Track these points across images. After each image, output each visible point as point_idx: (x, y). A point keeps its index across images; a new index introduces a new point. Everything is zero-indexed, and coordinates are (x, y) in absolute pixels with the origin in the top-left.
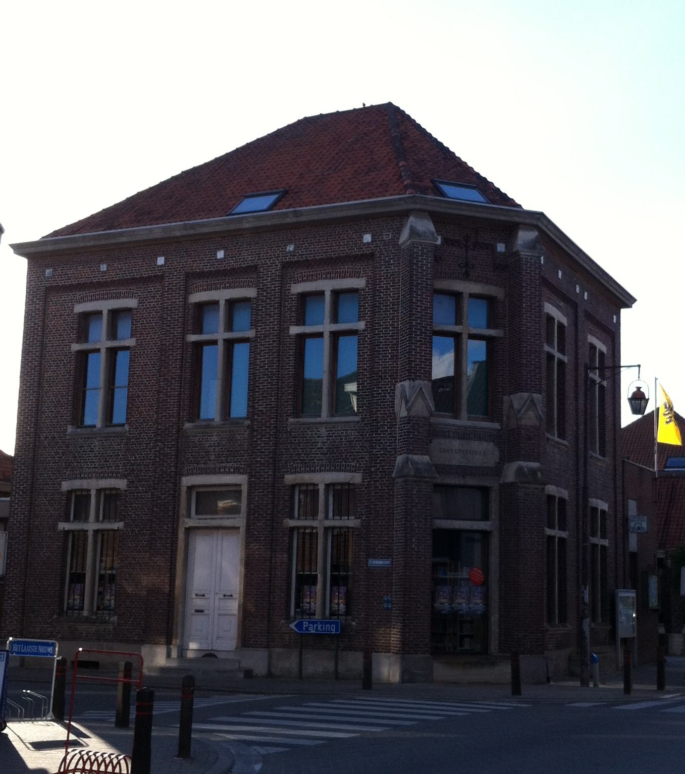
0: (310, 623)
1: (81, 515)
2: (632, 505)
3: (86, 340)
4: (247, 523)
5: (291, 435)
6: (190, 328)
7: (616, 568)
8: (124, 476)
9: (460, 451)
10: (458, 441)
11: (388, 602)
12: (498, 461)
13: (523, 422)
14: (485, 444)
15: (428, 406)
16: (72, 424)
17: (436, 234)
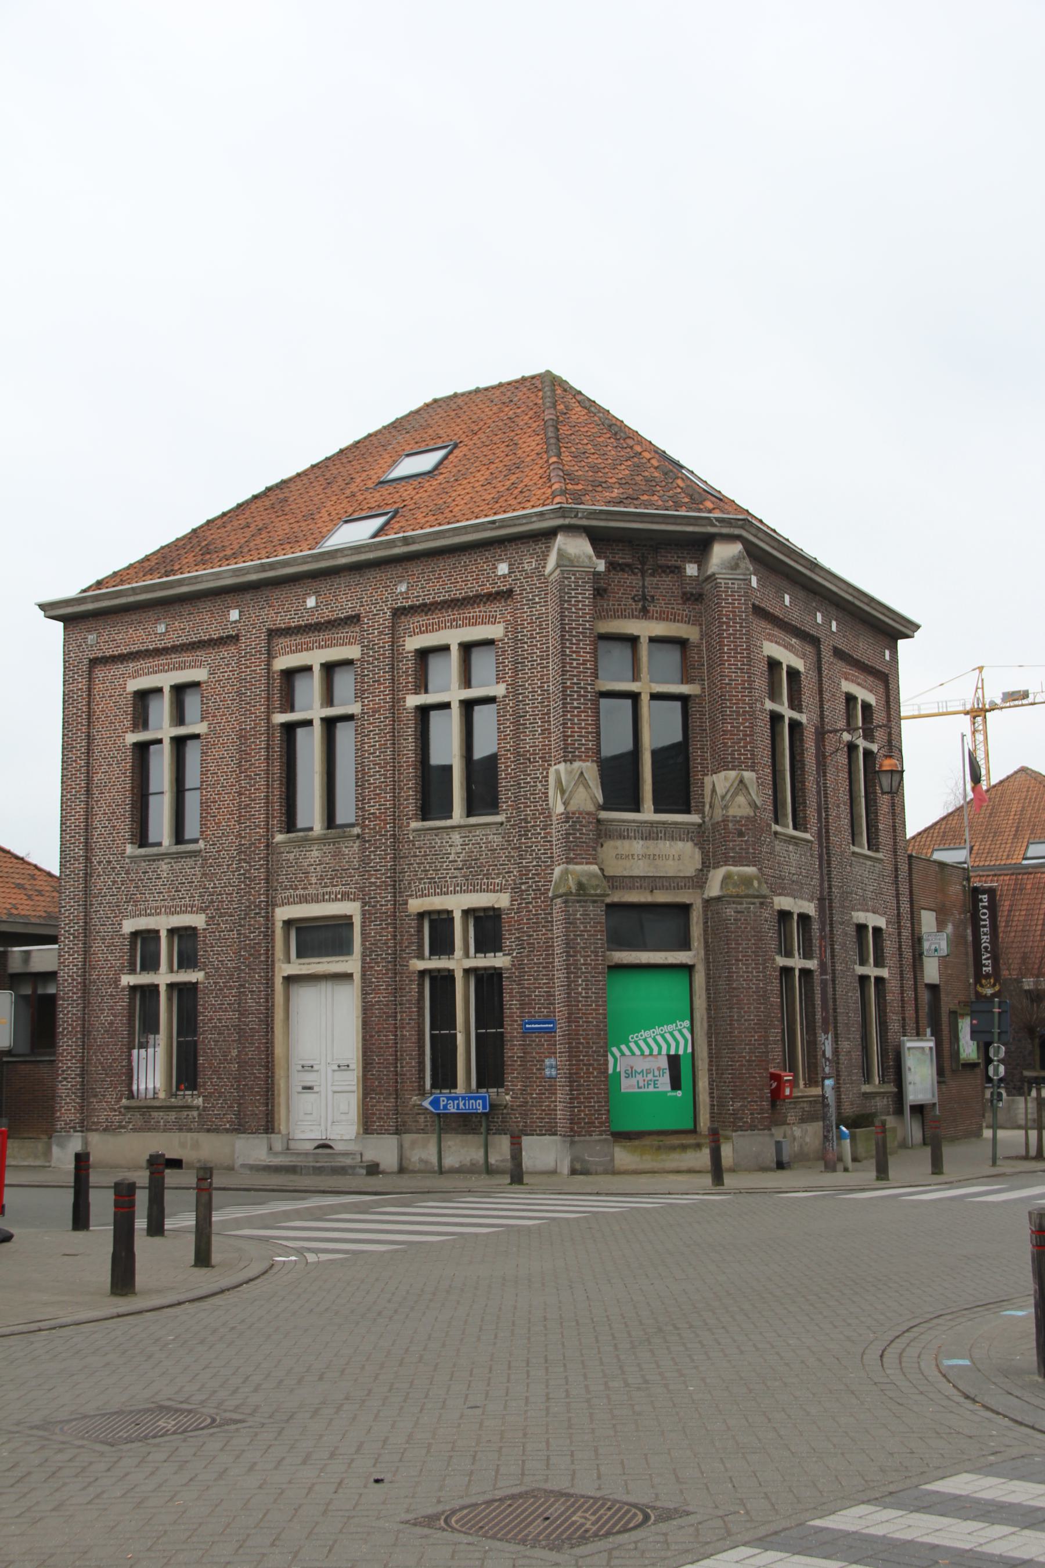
0: (448, 1098)
1: (150, 964)
2: (928, 920)
3: (145, 726)
4: (362, 967)
5: (414, 845)
6: (277, 704)
7: (903, 1007)
8: (203, 910)
9: (644, 856)
10: (641, 842)
11: (551, 1067)
12: (700, 867)
13: (731, 812)
14: (680, 844)
15: (593, 798)
16: (131, 843)
17: (594, 558)
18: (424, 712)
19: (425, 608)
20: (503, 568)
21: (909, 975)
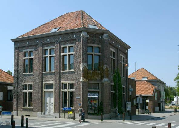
18: (63, 56)
19: (64, 41)
20: (75, 36)
21: (128, 93)
